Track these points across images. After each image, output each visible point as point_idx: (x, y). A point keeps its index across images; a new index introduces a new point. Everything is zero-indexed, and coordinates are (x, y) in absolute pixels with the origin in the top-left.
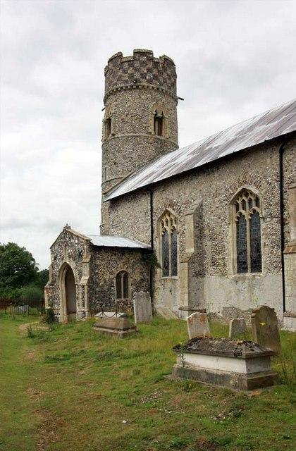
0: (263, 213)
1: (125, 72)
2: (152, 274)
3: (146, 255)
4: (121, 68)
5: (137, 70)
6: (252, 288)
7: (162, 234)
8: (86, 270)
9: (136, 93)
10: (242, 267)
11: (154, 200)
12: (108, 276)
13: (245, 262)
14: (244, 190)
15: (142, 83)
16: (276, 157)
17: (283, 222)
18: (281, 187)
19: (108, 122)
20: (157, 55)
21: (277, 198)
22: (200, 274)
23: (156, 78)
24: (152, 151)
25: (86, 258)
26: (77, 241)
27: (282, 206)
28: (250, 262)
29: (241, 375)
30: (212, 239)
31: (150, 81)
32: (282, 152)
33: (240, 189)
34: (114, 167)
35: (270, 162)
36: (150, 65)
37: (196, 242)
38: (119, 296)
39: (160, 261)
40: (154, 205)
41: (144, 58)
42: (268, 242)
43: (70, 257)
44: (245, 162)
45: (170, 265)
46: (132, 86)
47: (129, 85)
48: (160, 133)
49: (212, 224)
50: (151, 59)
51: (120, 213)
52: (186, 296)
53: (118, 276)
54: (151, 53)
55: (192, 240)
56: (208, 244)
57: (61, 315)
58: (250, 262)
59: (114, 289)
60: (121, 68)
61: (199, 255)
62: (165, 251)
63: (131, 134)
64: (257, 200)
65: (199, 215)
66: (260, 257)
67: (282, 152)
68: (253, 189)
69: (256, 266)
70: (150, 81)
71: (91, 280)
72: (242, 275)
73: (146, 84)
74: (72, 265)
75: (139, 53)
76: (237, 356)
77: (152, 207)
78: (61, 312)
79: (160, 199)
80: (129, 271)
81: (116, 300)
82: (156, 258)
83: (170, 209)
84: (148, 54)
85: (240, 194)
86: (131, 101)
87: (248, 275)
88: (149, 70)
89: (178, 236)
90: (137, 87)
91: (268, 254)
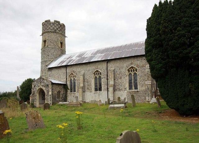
0: (102, 77)
1: (52, 26)
2: (66, 92)
3: (65, 86)
4: (50, 25)
5: (55, 27)
6: (99, 95)
7: (70, 80)
8: (50, 90)
9: (55, 34)
10: (96, 90)
11: (67, 70)
12: (56, 92)
13: (97, 89)
14: (97, 71)
15: (54, 32)
16: (106, 63)
17: (107, 79)
18: (107, 71)
19: (45, 41)
20: (52, 21)
21: (106, 74)
22: (84, 92)
23: (61, 30)
24: (60, 53)
25: (50, 86)
26: (46, 81)
27: (107, 76)
28: (98, 88)
29: (123, 106)
30: (87, 82)
31: (59, 31)
32: (107, 63)
33: (96, 70)
34: (48, 57)
35: (104, 65)
36: (59, 26)
37: (83, 83)
38: (58, 98)
39: (69, 88)
40: (67, 71)
41: (57, 23)
42: (104, 84)
43: (42, 86)
44: (97, 64)
45: (73, 89)
46: (54, 32)
47: (53, 31)
48: (61, 47)
49: (88, 78)
50: (59, 24)
51: (53, 72)
52: (81, 98)
53: (58, 93)
54: (59, 22)
55: (82, 82)
56: (86, 84)
57: (37, 104)
58: (98, 88)
59: (57, 96)
60: (50, 25)
61: (84, 86)
62: (71, 85)
63: (54, 47)
64: (101, 73)
65: (84, 76)
66: (101, 87)
67: (107, 63)
68: (100, 71)
69: (100, 89)
70: (59, 31)
71: (52, 94)
72: (96, 92)
73: (58, 32)
74: (44, 89)
75: (56, 22)
76: (123, 103)
77: (66, 72)
78: (37, 104)
79: (69, 70)
80: (61, 90)
81: (58, 99)
82: (68, 87)
83: (73, 73)
84: (59, 22)
85: (96, 71)
86: (53, 36)
87: (98, 92)
88: (59, 27)
89: (76, 81)
90: (56, 32)
91: (104, 87)
